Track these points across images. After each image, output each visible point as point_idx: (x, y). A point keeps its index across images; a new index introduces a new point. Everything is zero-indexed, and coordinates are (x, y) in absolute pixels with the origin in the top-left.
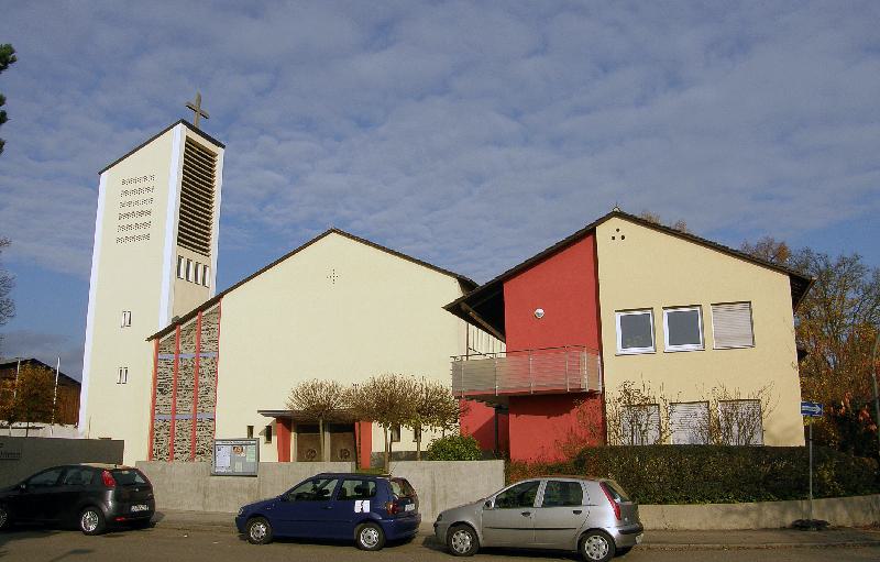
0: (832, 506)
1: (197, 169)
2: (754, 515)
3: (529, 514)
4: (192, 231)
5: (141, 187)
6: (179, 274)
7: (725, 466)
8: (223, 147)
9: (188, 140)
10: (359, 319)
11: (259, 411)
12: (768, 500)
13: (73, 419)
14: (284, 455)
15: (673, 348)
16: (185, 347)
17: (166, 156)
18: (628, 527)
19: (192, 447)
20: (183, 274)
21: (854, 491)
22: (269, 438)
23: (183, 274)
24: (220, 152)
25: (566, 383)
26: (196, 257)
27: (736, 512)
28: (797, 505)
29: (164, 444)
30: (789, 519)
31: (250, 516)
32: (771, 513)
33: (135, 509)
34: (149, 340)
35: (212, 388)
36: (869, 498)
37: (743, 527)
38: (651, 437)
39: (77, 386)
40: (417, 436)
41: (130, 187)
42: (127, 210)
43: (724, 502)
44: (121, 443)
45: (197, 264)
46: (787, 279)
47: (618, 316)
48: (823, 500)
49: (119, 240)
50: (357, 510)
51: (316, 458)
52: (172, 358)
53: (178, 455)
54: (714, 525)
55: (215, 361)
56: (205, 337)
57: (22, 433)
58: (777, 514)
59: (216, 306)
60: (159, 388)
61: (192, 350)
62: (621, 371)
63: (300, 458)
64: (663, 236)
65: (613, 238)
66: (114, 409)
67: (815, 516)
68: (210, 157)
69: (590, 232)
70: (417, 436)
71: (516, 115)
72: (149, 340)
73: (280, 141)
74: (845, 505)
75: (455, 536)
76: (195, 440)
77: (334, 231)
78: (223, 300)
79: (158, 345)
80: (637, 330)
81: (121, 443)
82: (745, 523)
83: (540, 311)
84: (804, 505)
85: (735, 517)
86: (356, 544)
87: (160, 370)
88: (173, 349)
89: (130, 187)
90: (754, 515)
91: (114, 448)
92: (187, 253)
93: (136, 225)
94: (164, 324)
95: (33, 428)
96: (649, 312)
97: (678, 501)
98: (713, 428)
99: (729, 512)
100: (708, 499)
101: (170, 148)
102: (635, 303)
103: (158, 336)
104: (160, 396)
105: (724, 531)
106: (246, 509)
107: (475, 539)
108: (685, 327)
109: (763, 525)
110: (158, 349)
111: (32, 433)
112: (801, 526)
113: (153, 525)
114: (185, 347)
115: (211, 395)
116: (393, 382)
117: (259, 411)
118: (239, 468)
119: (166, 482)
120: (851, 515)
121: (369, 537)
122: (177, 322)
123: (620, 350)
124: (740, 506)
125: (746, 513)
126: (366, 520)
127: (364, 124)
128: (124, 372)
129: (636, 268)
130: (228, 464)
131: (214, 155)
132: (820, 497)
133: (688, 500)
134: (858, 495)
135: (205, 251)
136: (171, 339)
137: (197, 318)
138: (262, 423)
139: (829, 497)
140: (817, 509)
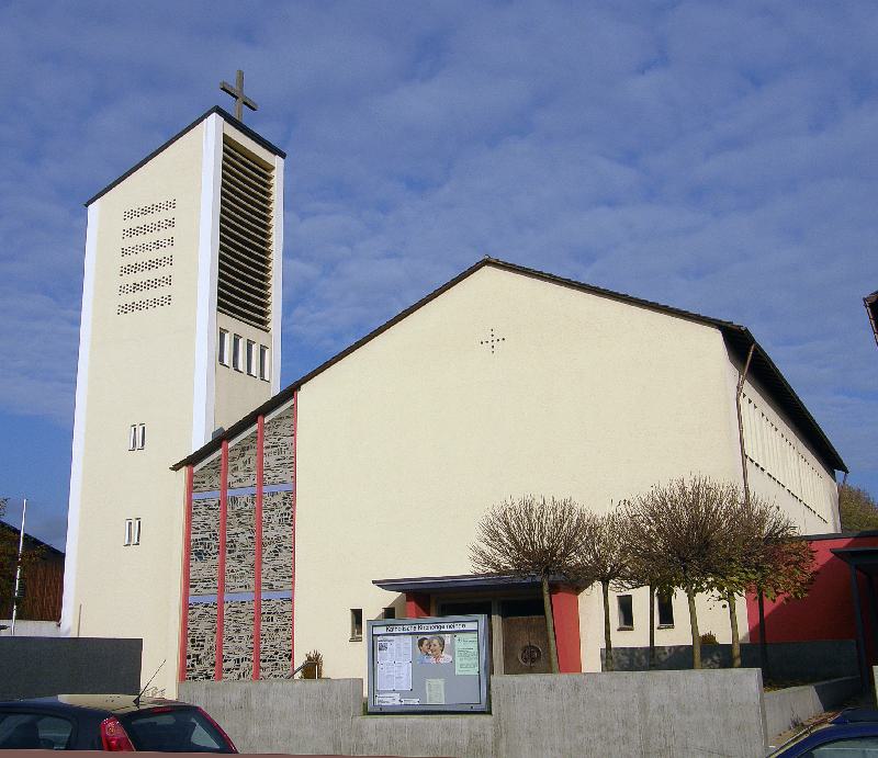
1: (243, 190)
4: (241, 289)
5: (154, 222)
6: (221, 359)
8: (283, 155)
9: (226, 140)
11: (374, 582)
13: (55, 616)
16: (238, 482)
17: (190, 173)
19: (256, 650)
20: (228, 359)
26: (247, 331)
29: (207, 646)
34: (176, 468)
35: (286, 546)
39: (57, 558)
42: (132, 259)
44: (140, 642)
46: (715, 338)
49: (125, 309)
51: (541, 663)
52: (217, 495)
53: (230, 664)
56: (271, 460)
59: (291, 402)
60: (194, 551)
61: (249, 482)
64: (563, 290)
66: (122, 583)
68: (265, 170)
71: (630, 158)
72: (176, 468)
78: (304, 394)
79: (191, 475)
81: (140, 642)
87: (228, 520)
88: (217, 481)
91: (120, 659)
92: (234, 325)
93: (146, 285)
94: (199, 441)
101: (201, 153)
103: (191, 461)
110: (192, 487)
114: (238, 482)
116: (529, 511)
117: (374, 582)
118: (436, 695)
122: (220, 439)
127: (418, 185)
128: (134, 533)
130: (406, 685)
135: (262, 323)
136: (215, 466)
137: (255, 427)
138: (376, 602)
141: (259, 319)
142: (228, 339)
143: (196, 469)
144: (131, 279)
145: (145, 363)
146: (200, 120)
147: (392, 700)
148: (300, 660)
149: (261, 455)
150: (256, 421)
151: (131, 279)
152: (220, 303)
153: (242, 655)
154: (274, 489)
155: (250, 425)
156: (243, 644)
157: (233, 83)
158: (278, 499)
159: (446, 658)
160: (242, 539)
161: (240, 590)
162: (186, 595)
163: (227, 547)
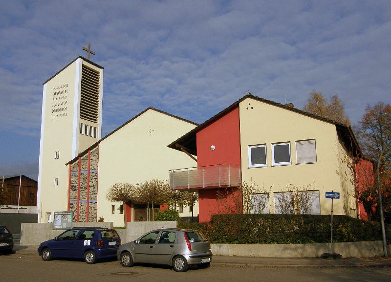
0: (348, 247)
1: (89, 79)
2: (300, 251)
3: (173, 246)
4: (88, 110)
6: (81, 132)
7: (302, 226)
8: (103, 68)
9: (83, 66)
10: (146, 152)
12: (310, 242)
14: (127, 219)
15: (277, 164)
16: (83, 165)
17: (71, 77)
18: (194, 255)
19: (88, 217)
20: (83, 132)
21: (364, 239)
22: (121, 213)
23: (83, 132)
24: (101, 71)
25: (219, 182)
26: (90, 123)
27: (290, 249)
28: (326, 246)
30: (321, 253)
31: (43, 248)
32: (311, 249)
33: (110, 244)
34: (66, 165)
36: (372, 243)
37: (293, 256)
38: (302, 211)
39: (35, 183)
40: (191, 209)
41: (57, 91)
43: (285, 243)
45: (91, 127)
47: (250, 148)
48: (343, 243)
50: (85, 244)
54: (277, 254)
55: (97, 175)
57: (17, 211)
58: (314, 250)
59: (97, 147)
60: (71, 188)
62: (252, 176)
63: (136, 220)
64: (267, 105)
65: (248, 109)
67: (337, 251)
69: (236, 106)
70: (191, 209)
71: (293, 43)
72: (66, 165)
73: (173, 63)
74: (356, 246)
75: (123, 257)
76: (88, 212)
77: (150, 108)
79: (71, 167)
80: (259, 155)
82: (294, 254)
83: (213, 147)
84: (330, 245)
85: (288, 251)
86: (84, 260)
89: (57, 91)
90: (300, 251)
92: (85, 122)
93: (60, 109)
94: (74, 157)
95: (22, 208)
96: (289, 143)
97: (260, 242)
98: (285, 207)
99: (286, 249)
100: (276, 241)
101: (76, 68)
102: (257, 141)
103: (71, 163)
104: (72, 192)
105: (282, 258)
106: (42, 244)
107: (131, 259)
108: (282, 153)
109: (305, 255)
110: (71, 170)
111: (26, 212)
112: (325, 256)
113: (14, 253)
114: (83, 165)
115: (95, 191)
119: (34, 232)
120: (360, 251)
121: (90, 257)
123: (251, 166)
124: (293, 246)
125: (296, 249)
126: (88, 249)
127: (215, 52)
129: (259, 124)
131: (98, 73)
132: (341, 242)
133: (266, 242)
134: (366, 241)
135: (95, 121)
137: (88, 154)
139: (346, 241)
140: (339, 248)
141: (94, 119)
142: (83, 126)
143: (72, 165)
144: (64, 106)
145: (59, 132)
146: (75, 60)
147: (57, 227)
148: (98, 219)
149: (90, 161)
150: (88, 152)
151: (64, 106)
152: (80, 115)
153: (84, 217)
154: (93, 171)
155: (87, 153)
156: (84, 215)
157: (87, 47)
158: (94, 174)
159: (67, 219)
160: (84, 185)
161: (83, 200)
162: (69, 201)
163: (80, 187)
